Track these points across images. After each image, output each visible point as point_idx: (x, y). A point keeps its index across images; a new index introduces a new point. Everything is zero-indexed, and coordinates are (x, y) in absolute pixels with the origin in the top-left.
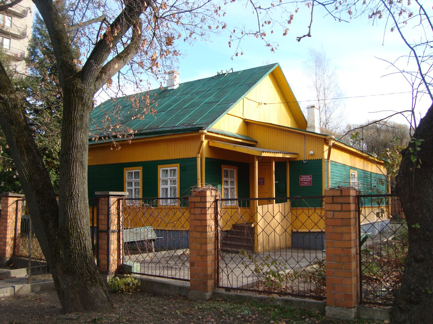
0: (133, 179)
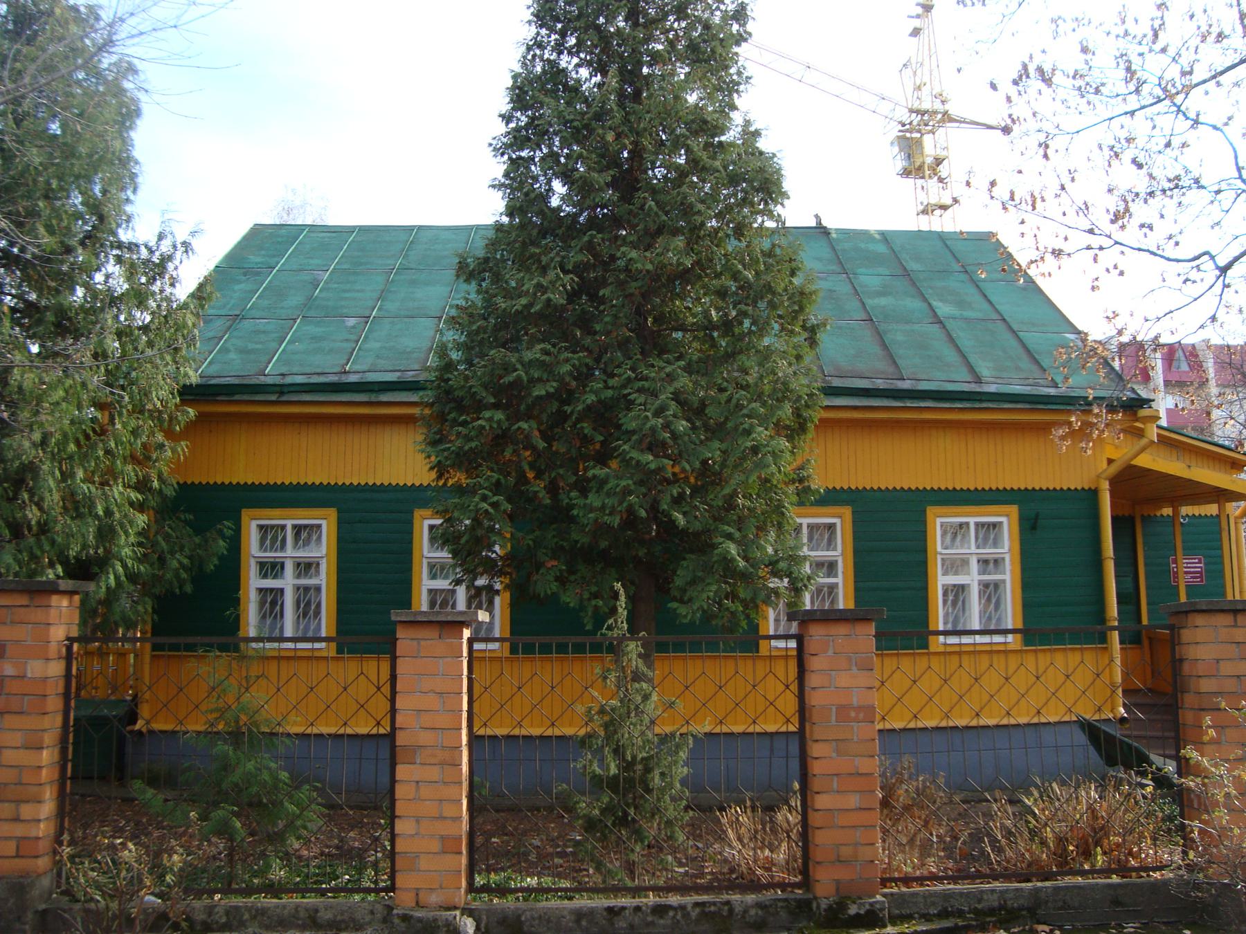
0: (973, 549)
